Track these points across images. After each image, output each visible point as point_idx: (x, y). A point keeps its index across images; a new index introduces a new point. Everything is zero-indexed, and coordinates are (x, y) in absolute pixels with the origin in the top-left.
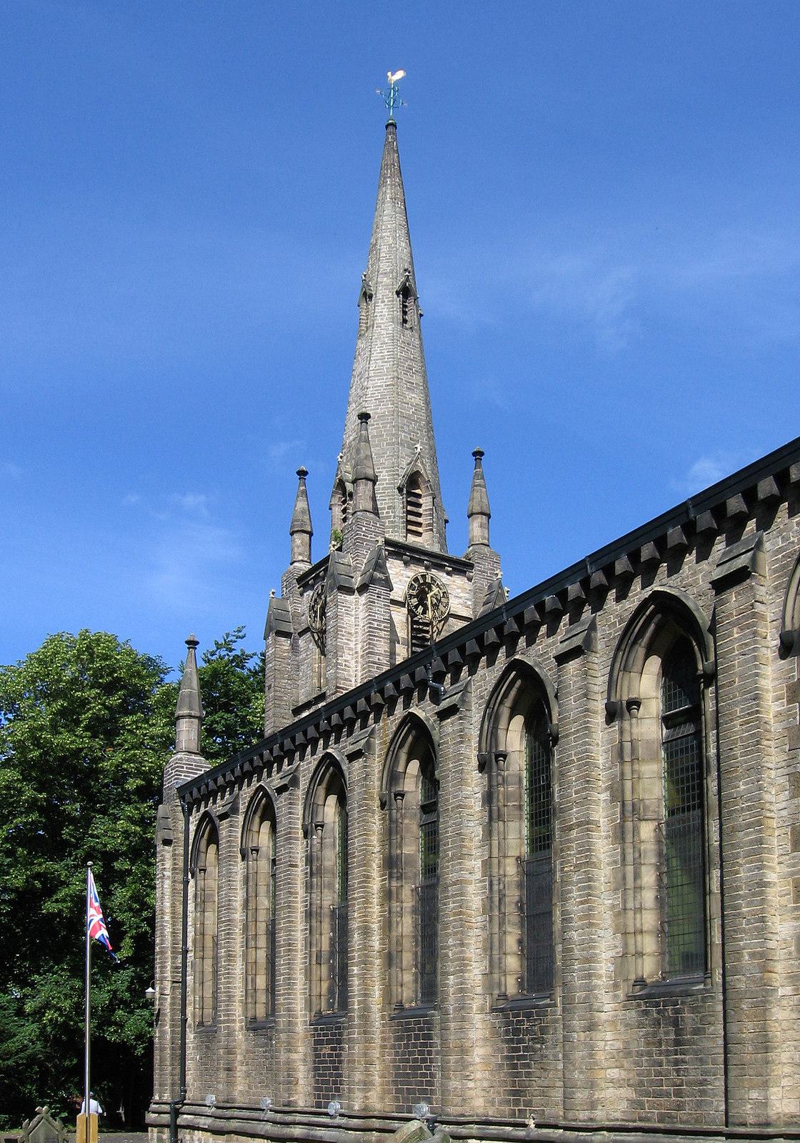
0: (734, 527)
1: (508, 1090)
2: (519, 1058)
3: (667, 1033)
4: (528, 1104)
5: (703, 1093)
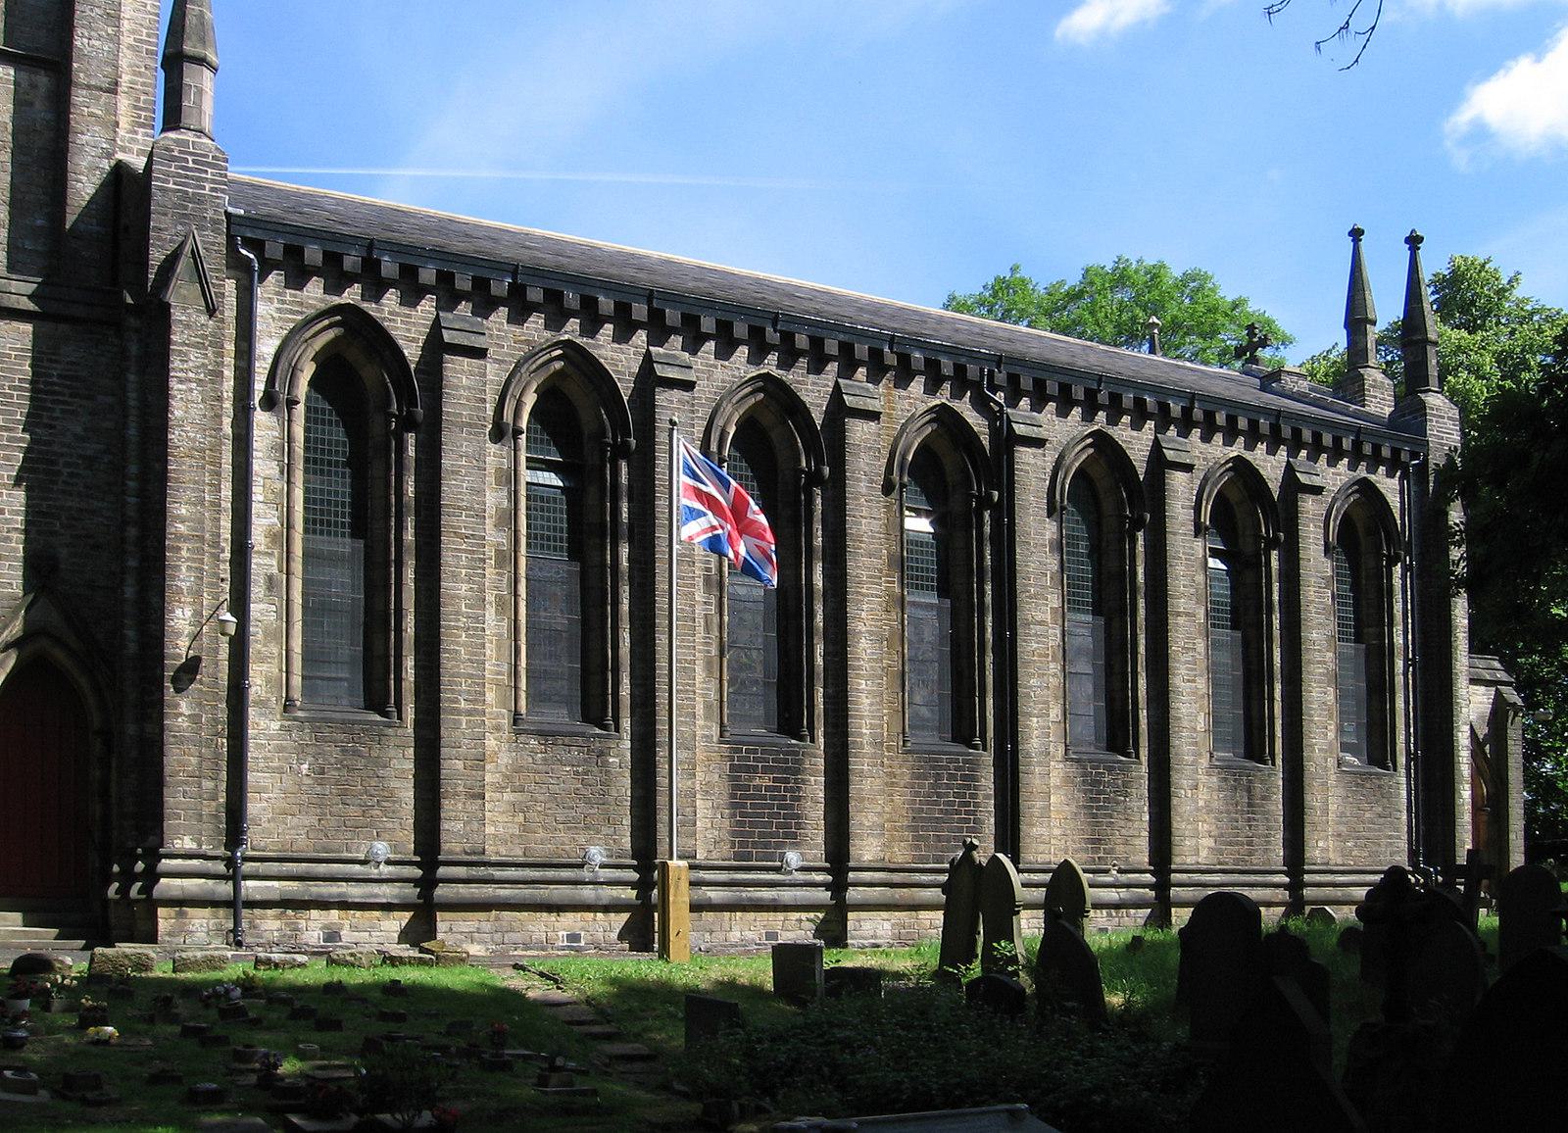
0: (485, 305)
1: (1084, 839)
2: (1098, 808)
3: (1242, 797)
4: (1111, 851)
5: (1268, 843)
